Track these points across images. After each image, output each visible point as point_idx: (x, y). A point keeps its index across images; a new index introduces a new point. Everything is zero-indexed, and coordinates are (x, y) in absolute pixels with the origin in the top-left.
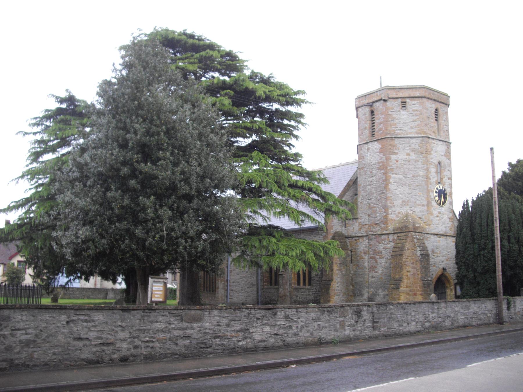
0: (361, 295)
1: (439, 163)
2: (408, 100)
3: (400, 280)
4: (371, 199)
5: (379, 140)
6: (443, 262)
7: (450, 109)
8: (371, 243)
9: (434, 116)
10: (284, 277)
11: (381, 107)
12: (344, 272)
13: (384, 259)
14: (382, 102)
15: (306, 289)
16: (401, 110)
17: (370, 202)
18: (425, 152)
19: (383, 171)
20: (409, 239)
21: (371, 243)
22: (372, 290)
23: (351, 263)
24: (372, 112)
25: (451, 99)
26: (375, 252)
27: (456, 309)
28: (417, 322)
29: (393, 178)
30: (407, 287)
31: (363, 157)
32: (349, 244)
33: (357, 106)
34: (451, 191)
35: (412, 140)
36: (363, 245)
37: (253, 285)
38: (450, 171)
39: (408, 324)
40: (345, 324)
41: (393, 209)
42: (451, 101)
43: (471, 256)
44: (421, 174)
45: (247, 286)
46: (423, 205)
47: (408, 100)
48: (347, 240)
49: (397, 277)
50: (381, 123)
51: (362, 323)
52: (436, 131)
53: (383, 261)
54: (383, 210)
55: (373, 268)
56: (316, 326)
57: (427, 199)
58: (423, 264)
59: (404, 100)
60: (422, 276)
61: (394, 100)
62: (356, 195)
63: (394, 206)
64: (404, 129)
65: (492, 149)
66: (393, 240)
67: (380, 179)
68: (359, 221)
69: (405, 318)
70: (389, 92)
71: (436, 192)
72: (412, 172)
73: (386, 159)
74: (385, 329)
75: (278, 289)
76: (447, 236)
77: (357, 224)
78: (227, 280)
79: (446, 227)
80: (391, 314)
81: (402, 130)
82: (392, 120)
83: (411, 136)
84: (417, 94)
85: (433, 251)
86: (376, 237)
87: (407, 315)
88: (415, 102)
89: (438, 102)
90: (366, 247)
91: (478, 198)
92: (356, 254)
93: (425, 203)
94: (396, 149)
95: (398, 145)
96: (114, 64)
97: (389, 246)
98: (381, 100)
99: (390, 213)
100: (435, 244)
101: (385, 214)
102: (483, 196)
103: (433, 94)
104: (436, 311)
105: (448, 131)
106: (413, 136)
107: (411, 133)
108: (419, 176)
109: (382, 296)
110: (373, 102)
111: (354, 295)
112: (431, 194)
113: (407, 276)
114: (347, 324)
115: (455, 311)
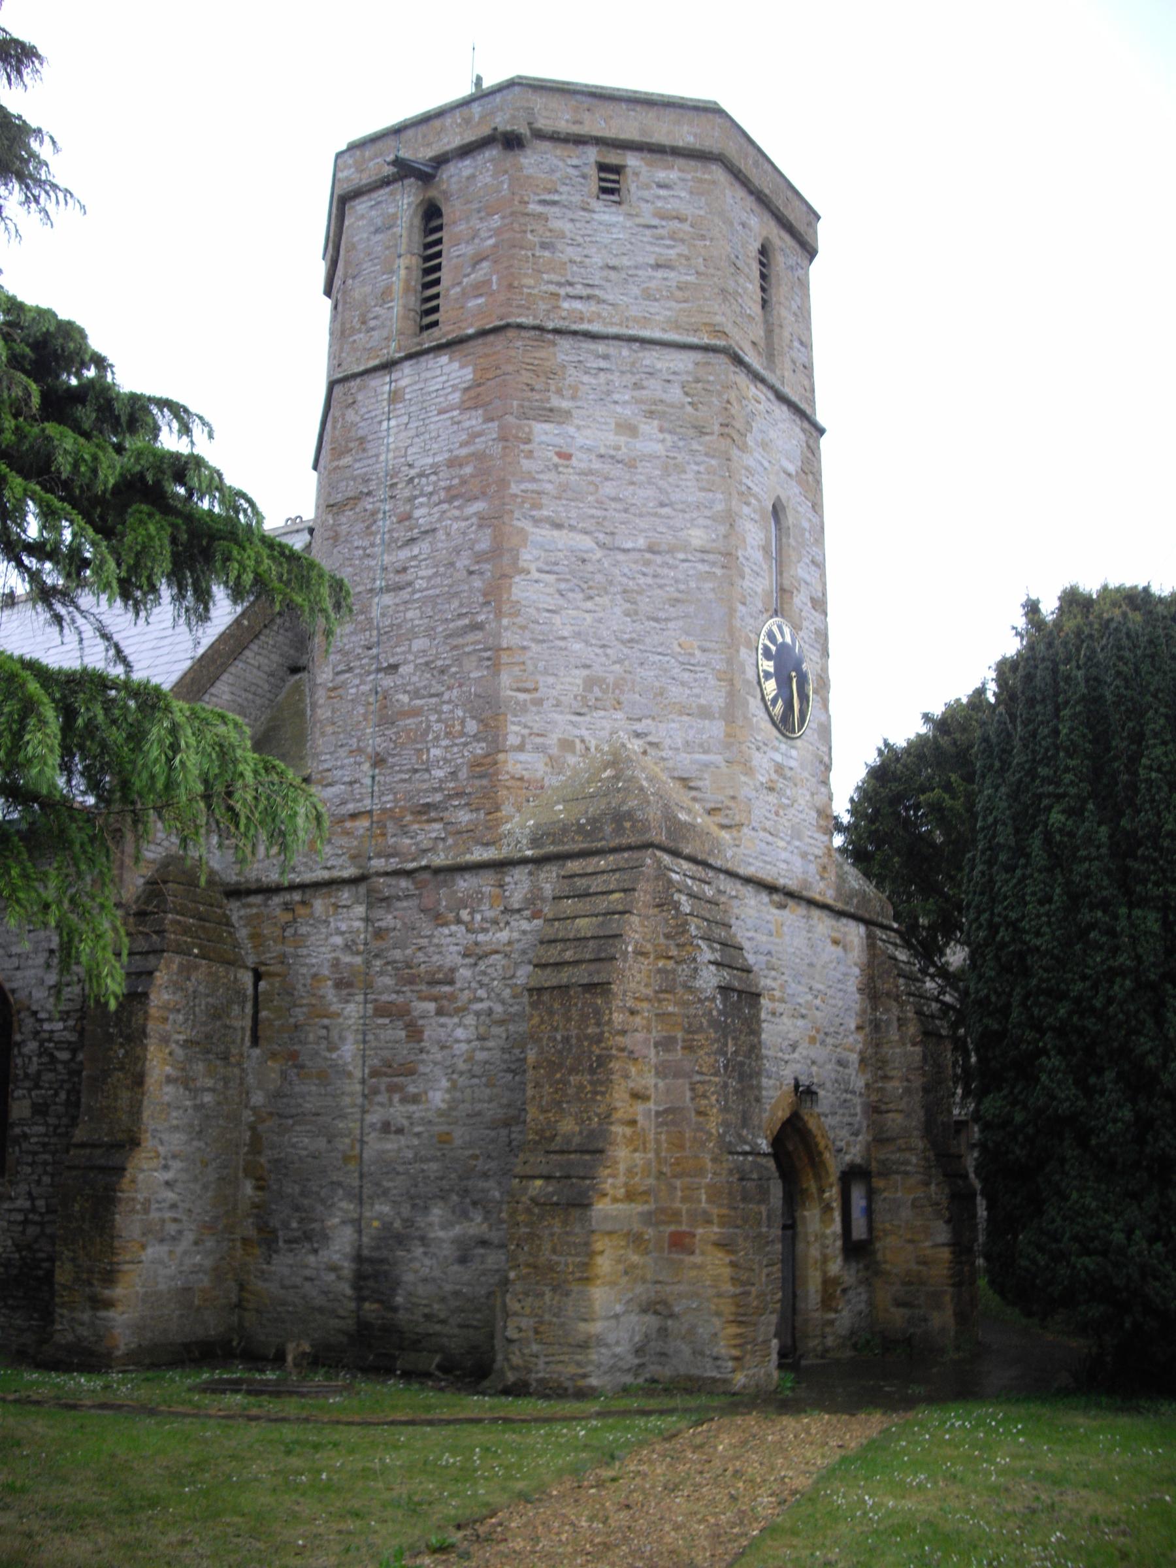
0: (308, 1237)
2: (632, 161)
3: (594, 1148)
4: (393, 668)
7: (817, 270)
8: (388, 920)
9: (755, 268)
11: (485, 178)
12: (208, 1098)
13: (470, 1020)
14: (492, 152)
16: (595, 204)
17: (387, 681)
19: (479, 506)
20: (643, 895)
21: (388, 920)
23: (255, 1041)
24: (431, 215)
25: (821, 226)
26: (407, 976)
29: (538, 544)
30: (630, 1196)
31: (362, 440)
32: (243, 933)
33: (346, 187)
34: (825, 669)
35: (652, 358)
36: (333, 935)
41: (534, 719)
43: (1121, 987)
44: (696, 543)
46: (704, 713)
48: (236, 911)
49: (568, 1126)
50: (477, 261)
53: (462, 1032)
54: (472, 726)
55: (392, 1074)
58: (731, 1048)
59: (613, 158)
60: (726, 1124)
61: (560, 150)
62: (295, 670)
63: (539, 702)
64: (610, 297)
70: (538, 102)
71: (767, 654)
72: (642, 524)
79: (804, 855)
81: (600, 301)
82: (544, 246)
83: (646, 333)
84: (685, 135)
86: (420, 886)
90: (347, 947)
91: (943, 725)
92: (288, 991)
93: (716, 698)
94: (559, 392)
97: (504, 936)
99: (513, 740)
101: (479, 749)
102: (919, 749)
106: (657, 334)
107: (646, 321)
108: (685, 547)
109: (448, 1250)
110: (441, 161)
111: (268, 1238)
112: (744, 652)
113: (633, 1123)
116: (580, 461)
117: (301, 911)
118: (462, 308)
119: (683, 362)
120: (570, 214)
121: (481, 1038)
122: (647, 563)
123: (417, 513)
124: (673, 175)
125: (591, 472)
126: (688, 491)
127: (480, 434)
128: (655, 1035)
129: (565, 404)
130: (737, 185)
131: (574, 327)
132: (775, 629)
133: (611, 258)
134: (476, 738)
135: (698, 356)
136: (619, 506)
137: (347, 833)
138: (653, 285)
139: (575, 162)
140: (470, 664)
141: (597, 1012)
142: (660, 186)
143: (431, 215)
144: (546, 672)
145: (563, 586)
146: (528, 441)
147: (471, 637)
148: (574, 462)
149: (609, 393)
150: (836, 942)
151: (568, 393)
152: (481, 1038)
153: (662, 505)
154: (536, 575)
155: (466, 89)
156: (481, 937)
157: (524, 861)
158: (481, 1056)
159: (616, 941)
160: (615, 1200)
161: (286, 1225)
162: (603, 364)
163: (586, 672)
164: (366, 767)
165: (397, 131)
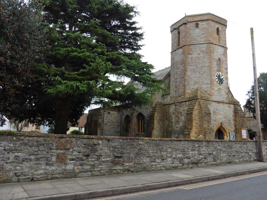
1: (219, 59)
2: (199, 23)
5: (182, 47)
8: (177, 107)
11: (183, 28)
13: (183, 117)
17: (176, 83)
18: (209, 52)
19: (183, 65)
20: (197, 103)
24: (179, 32)
27: (219, 147)
28: (174, 158)
29: (189, 68)
35: (201, 46)
38: (227, 64)
39: (163, 160)
40: (66, 158)
41: (189, 86)
42: (228, 24)
46: (208, 84)
51: (96, 157)
54: (183, 88)
55: (177, 122)
59: (197, 23)
63: (189, 85)
65: (252, 29)
66: (188, 105)
69: (159, 154)
70: (188, 18)
71: (217, 76)
73: (185, 58)
74: (131, 164)
76: (224, 103)
77: (169, 97)
80: (140, 149)
82: (189, 35)
84: (205, 18)
85: (214, 112)
87: (161, 151)
93: (209, 82)
97: (186, 108)
98: (183, 24)
100: (216, 107)
103: (216, 18)
105: (225, 41)
106: (203, 43)
115: (218, 150)
116: (194, 59)
119: (206, 45)
126: (206, 60)
129: (192, 53)
130: (213, 22)
131: (193, 44)
133: (196, 34)
135: (207, 44)
136: (198, 63)
137: (173, 99)
138: (202, 37)
141: (192, 116)
143: (179, 32)
145: (192, 72)
146: (188, 57)
153: (203, 62)
155: (184, 16)
157: (188, 101)
159: (193, 109)
164: (175, 92)
165: (175, 24)
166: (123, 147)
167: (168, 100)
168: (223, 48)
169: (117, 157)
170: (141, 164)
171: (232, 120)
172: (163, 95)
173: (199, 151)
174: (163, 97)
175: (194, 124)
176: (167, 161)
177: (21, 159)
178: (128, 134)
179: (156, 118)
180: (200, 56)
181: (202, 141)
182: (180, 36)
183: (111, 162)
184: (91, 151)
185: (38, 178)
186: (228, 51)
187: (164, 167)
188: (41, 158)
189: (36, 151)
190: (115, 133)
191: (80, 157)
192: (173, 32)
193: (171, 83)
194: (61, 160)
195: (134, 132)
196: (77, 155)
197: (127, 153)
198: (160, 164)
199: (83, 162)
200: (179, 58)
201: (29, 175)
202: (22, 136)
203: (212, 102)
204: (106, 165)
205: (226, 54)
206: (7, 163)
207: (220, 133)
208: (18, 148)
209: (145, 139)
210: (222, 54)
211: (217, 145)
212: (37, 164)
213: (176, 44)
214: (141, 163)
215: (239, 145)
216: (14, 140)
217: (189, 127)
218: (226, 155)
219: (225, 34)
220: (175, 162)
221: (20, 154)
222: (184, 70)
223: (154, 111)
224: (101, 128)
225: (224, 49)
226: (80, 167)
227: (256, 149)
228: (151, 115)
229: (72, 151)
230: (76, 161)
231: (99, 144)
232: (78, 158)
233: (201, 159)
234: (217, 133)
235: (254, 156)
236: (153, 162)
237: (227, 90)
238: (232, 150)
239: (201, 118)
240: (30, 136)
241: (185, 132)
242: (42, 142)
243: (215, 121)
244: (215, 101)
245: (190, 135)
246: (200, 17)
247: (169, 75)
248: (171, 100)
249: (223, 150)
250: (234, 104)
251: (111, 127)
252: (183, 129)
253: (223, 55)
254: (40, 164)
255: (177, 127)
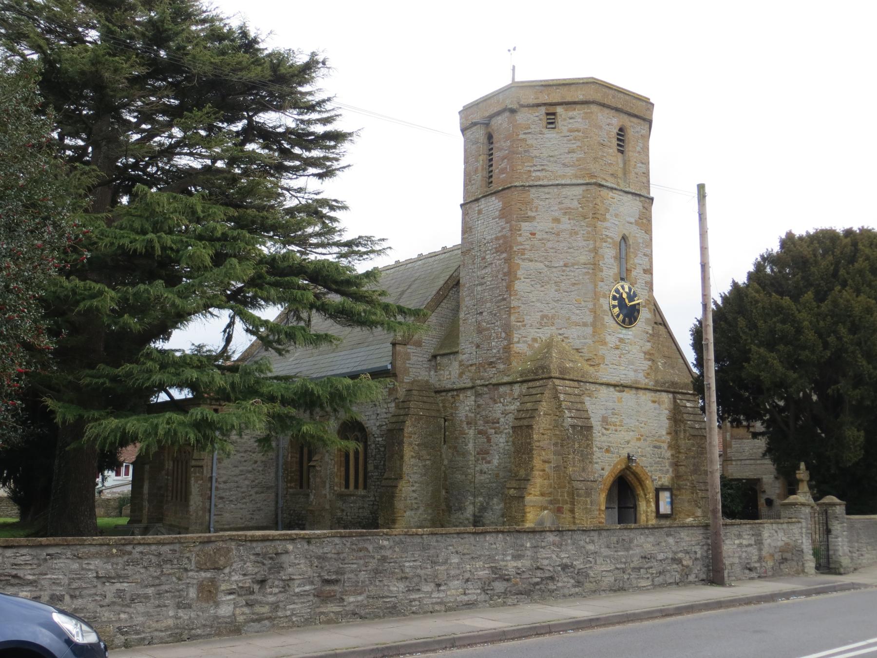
1: (624, 238)
2: (559, 110)
4: (481, 313)
6: (628, 442)
10: (317, 471)
11: (505, 125)
13: (504, 436)
14: (507, 114)
15: (357, 496)
16: (545, 131)
18: (594, 215)
19: (504, 255)
20: (547, 394)
21: (481, 402)
22: (481, 499)
24: (490, 137)
27: (591, 547)
28: (467, 580)
29: (524, 268)
35: (565, 191)
36: (466, 405)
37: (268, 488)
38: (650, 256)
39: (439, 585)
40: (217, 589)
41: (522, 331)
44: (582, 261)
45: (256, 489)
46: (585, 325)
47: (559, 110)
51: (281, 584)
52: (620, 174)
54: (503, 335)
55: (483, 454)
56: (110, 595)
57: (594, 311)
59: (551, 110)
63: (524, 326)
65: (701, 188)
66: (519, 396)
67: (498, 271)
68: (461, 357)
69: (429, 571)
71: (614, 298)
73: (511, 230)
74: (360, 598)
75: (307, 496)
76: (637, 388)
77: (456, 364)
78: (211, 478)
79: (635, 371)
80: (384, 559)
82: (525, 151)
83: (563, 182)
87: (434, 563)
88: (577, 112)
89: (625, 116)
93: (589, 319)
94: (531, 210)
95: (536, 202)
96: (390, 248)
99: (516, 340)
100: (610, 404)
101: (505, 343)
103: (614, 97)
104: (529, 553)
105: (646, 174)
106: (569, 182)
107: (564, 176)
112: (602, 300)
113: (544, 470)
114: (223, 587)
115: (587, 554)
117: (457, 398)
118: (500, 179)
119: (579, 191)
120: (535, 137)
121: (507, 442)
122: (564, 271)
123: (487, 257)
124: (575, 113)
125: (543, 239)
127: (504, 228)
128: (553, 442)
129: (533, 214)
130: (605, 109)
131: (536, 183)
132: (620, 288)
134: (505, 339)
135: (584, 188)
137: (469, 371)
139: (537, 114)
140: (503, 312)
141: (530, 435)
142: (571, 118)
143: (490, 137)
144: (527, 314)
146: (520, 230)
147: (503, 303)
148: (537, 236)
149: (550, 207)
150: (654, 402)
151: (534, 210)
152: (507, 442)
153: (569, 248)
154: (523, 280)
156: (507, 408)
158: (507, 448)
160: (535, 495)
161: (454, 505)
162: (548, 196)
163: (541, 314)
166: (342, 556)
167: (450, 374)
168: (638, 198)
169: (328, 582)
170: (383, 597)
171: (666, 448)
172: (435, 357)
173: (535, 559)
174: (433, 363)
175: (537, 462)
176: (449, 589)
177: (128, 596)
178: (308, 495)
179: (410, 437)
180: (561, 226)
181: (542, 531)
182: (492, 149)
183: (314, 596)
184: (270, 569)
185: (161, 638)
186: (657, 211)
187: (441, 603)
188: (167, 592)
189: (158, 578)
190: (257, 493)
191: (247, 585)
192: (468, 133)
193: (462, 315)
194: (209, 592)
195: (328, 486)
196: (240, 581)
197: (352, 571)
198: (430, 597)
199: (252, 597)
200: (490, 228)
201: (143, 632)
202: (129, 544)
203: (597, 386)
204: (304, 603)
205: (649, 221)
206: (102, 606)
207: (625, 489)
208: (123, 572)
209: (395, 533)
210: (633, 220)
211: (587, 540)
212: (159, 606)
213: (479, 177)
214: (386, 594)
215: (651, 539)
216: (113, 555)
217: (522, 473)
218: (613, 567)
219: (646, 149)
220: (470, 592)
221: (126, 584)
222: (505, 274)
223: (402, 412)
224: (202, 473)
225: (640, 204)
226: (246, 610)
227: (705, 548)
228: (390, 427)
229: (230, 573)
230: (239, 595)
231: (287, 552)
232: (242, 587)
233: (539, 580)
234: (616, 491)
235: (698, 570)
236: (413, 590)
237: (649, 344)
238: (631, 552)
239: (562, 442)
240: (144, 544)
241: (512, 486)
242: (170, 556)
243: (608, 451)
244: (608, 385)
245: (523, 502)
246: (563, 91)
247: (454, 284)
248: (461, 374)
249: (605, 554)
250: (672, 390)
251: (241, 471)
252: (504, 477)
253: (637, 223)
254: (165, 606)
255: (481, 471)
